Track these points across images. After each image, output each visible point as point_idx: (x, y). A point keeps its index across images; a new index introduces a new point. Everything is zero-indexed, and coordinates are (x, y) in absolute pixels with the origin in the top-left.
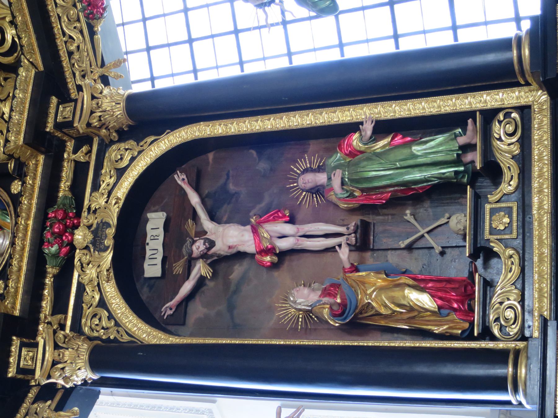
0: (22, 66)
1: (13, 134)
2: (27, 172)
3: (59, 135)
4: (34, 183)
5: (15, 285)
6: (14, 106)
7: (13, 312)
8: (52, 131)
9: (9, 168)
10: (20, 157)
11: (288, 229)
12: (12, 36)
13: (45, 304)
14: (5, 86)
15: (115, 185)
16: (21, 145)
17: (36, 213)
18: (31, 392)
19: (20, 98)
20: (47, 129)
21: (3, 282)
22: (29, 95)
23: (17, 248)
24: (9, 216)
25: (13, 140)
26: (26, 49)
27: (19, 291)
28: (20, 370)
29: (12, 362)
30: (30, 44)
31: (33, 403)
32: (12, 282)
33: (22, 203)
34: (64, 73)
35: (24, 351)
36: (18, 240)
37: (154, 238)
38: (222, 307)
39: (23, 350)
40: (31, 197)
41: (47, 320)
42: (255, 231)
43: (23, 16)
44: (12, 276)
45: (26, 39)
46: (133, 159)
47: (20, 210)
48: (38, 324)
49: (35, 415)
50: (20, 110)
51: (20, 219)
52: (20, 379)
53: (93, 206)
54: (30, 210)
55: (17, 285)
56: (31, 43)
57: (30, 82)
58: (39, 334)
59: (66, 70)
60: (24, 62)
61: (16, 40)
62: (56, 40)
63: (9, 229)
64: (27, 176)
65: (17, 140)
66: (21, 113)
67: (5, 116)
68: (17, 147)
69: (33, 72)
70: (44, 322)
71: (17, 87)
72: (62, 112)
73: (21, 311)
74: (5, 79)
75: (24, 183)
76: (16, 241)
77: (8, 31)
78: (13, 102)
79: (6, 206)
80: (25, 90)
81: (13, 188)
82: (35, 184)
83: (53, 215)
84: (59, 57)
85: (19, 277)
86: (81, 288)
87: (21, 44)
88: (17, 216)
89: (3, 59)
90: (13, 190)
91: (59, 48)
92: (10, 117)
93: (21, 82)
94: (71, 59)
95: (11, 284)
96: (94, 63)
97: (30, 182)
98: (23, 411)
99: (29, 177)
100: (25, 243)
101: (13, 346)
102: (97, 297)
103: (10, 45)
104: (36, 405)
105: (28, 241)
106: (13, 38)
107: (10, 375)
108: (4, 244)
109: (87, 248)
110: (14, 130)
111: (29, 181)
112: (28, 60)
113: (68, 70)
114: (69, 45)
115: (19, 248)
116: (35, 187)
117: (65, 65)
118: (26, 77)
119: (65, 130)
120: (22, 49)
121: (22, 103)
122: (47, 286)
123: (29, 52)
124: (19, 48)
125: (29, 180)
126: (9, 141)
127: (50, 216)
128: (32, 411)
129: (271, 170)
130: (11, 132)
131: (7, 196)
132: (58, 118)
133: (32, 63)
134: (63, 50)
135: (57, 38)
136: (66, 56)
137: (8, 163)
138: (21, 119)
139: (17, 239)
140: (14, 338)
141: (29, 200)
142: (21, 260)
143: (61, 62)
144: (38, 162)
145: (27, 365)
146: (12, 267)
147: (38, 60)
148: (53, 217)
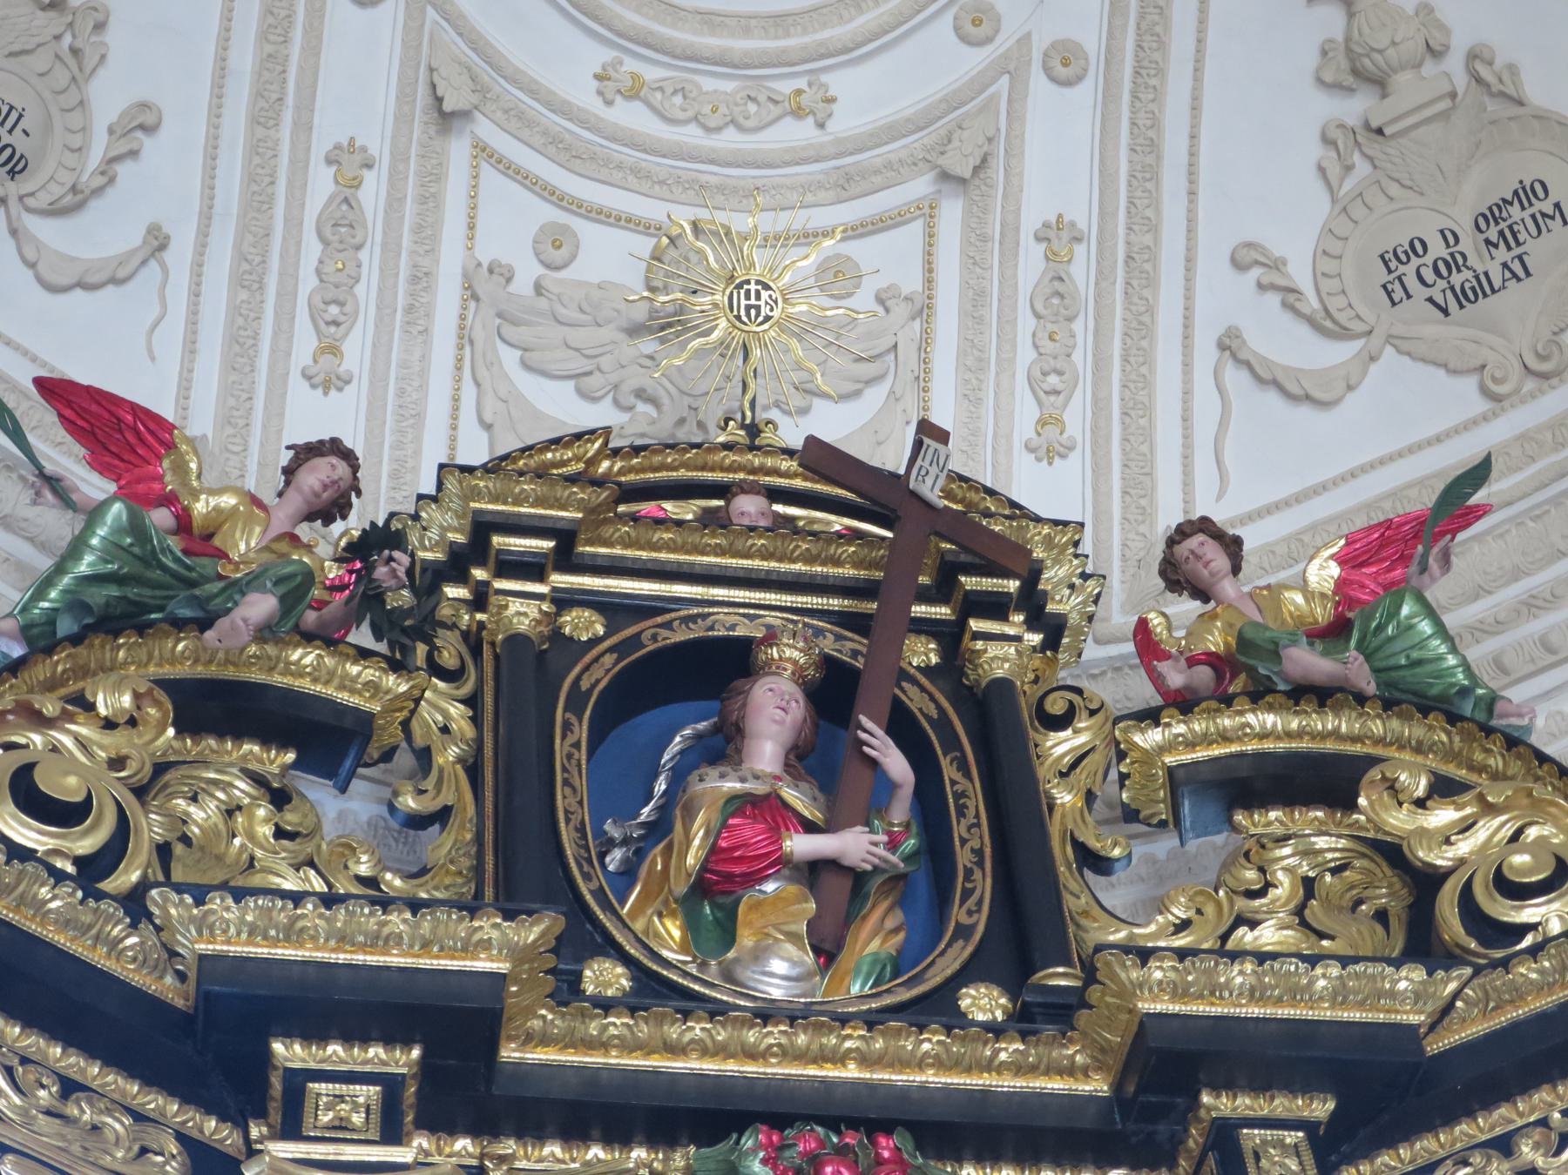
0: (1430, 974)
1: (1172, 975)
2: (1038, 1040)
3: (1191, 1143)
4: (1000, 1069)
5: (615, 1036)
6: (1277, 965)
7: (510, 1039)
8: (1203, 1113)
9: (1051, 970)
10: (1091, 1007)
12: (1540, 923)
13: (553, 1154)
14: (1355, 919)
16: (1135, 1005)
17: (889, 1087)
18: (222, 1126)
19: (1311, 983)
20: (1210, 1094)
21: (624, 990)
22: (1328, 1015)
23: (751, 1033)
24: (871, 988)
25: (1150, 975)
26: (1498, 979)
27: (591, 1056)
28: (298, 1081)
29: (325, 1050)
30: (1518, 994)
31: (181, 1138)
32: (622, 1024)
33: (921, 1033)
34: (1429, 1131)
35: (368, 1093)
36: (780, 1032)
39: (371, 1088)
40: (947, 1062)
41: (491, 1166)
43: (1540, 988)
44: (646, 1023)
45: (1534, 976)
47: (892, 1028)
48: (474, 1132)
49: (136, 1148)
50: (1264, 987)
51: (862, 1033)
52: (265, 1084)
54: (898, 1067)
55: (615, 1046)
56: (1522, 998)
57: (1379, 1011)
58: (439, 1139)
59: (1442, 1137)
60: (1449, 980)
61: (1528, 941)
62: (1546, 1087)
63: (823, 997)
64: (1023, 1041)
65: (1151, 990)
66: (1255, 994)
67: (1242, 930)
68: (1127, 993)
69: (1414, 1019)
70: (482, 1156)
71: (1350, 968)
72: (1280, 1144)
73: (518, 1065)
74: (1381, 916)
75: (996, 1031)
76: (776, 1025)
77: (1556, 905)
78: (1294, 960)
79: (914, 972)
80: (1345, 998)
81: (978, 991)
82: (999, 1073)
83: (886, 1154)
84: (1488, 1104)
85: (646, 1049)
87: (1515, 961)
88: (872, 1021)
89: (1452, 902)
90: (973, 992)
91: (1518, 1099)
92: (1236, 956)
93: (1373, 977)
94: (1482, 1151)
95: (617, 1023)
97: (1003, 1056)
98: (149, 1103)
99: (1022, 1047)
100: (773, 1060)
101: (386, 1052)
103: (1505, 919)
104: (173, 1147)
105: (780, 1071)
106: (1533, 927)
107: (278, 1047)
108: (766, 979)
110: (1190, 973)
111: (1006, 1049)
112: (1457, 995)
113: (1442, 1146)
114: (1537, 1138)
115: (752, 1040)
116: (986, 1075)
117: (1461, 1132)
118: (1392, 994)
119: (1211, 1161)
120: (1494, 965)
121: (1295, 994)
122: (621, 1154)
123: (1486, 992)
124: (1498, 954)
125: (1009, 1050)
126: (1144, 963)
127: (883, 1141)
128: (153, 1137)
130: (1180, 966)
131: (949, 972)
132: (1256, 1132)
133: (1449, 1007)
134: (1514, 1117)
135: (1555, 1087)
136: (1492, 1128)
137: (1068, 962)
138: (1231, 995)
139: (783, 1028)
140: (416, 1053)
141: (937, 1056)
142: (705, 1052)
143: (1470, 1114)
144: (1080, 1076)
145: (317, 1108)
146: (677, 1019)
147: (1463, 1029)
148: (878, 1155)
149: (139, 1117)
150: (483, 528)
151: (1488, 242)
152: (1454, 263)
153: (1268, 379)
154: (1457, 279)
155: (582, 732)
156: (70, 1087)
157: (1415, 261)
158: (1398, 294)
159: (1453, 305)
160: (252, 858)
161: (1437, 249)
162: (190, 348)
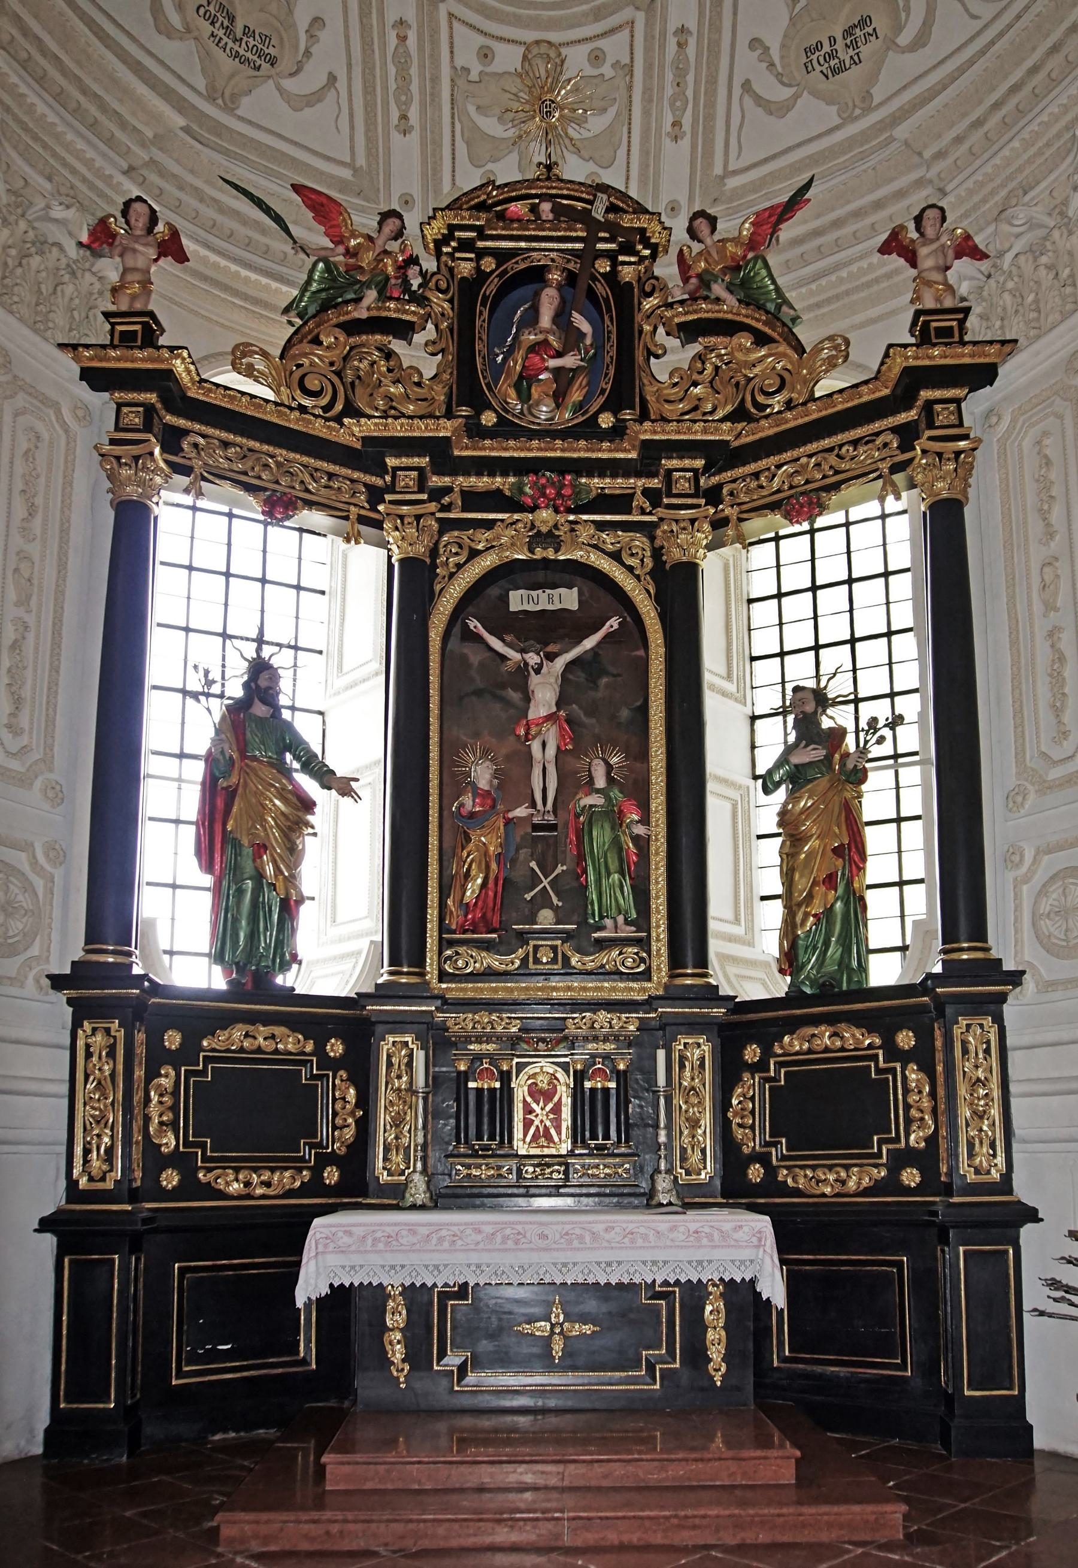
11: (551, 751)
15: (603, 551)
31: (365, 485)
37: (550, 599)
38: (479, 683)
42: (549, 718)
46: (630, 569)
53: (579, 526)
69: (728, 438)
86: (489, 525)
96: (745, 507)
102: (480, 547)
107: (387, 460)
109: (533, 526)
129: (620, 724)
149: (352, 481)
150: (452, 228)
151: (846, 45)
152: (832, 55)
153: (759, 100)
154: (832, 63)
155: (486, 314)
156: (331, 476)
157: (817, 53)
158: (810, 68)
159: (830, 75)
160: (380, 381)
161: (827, 48)
162: (352, 127)
